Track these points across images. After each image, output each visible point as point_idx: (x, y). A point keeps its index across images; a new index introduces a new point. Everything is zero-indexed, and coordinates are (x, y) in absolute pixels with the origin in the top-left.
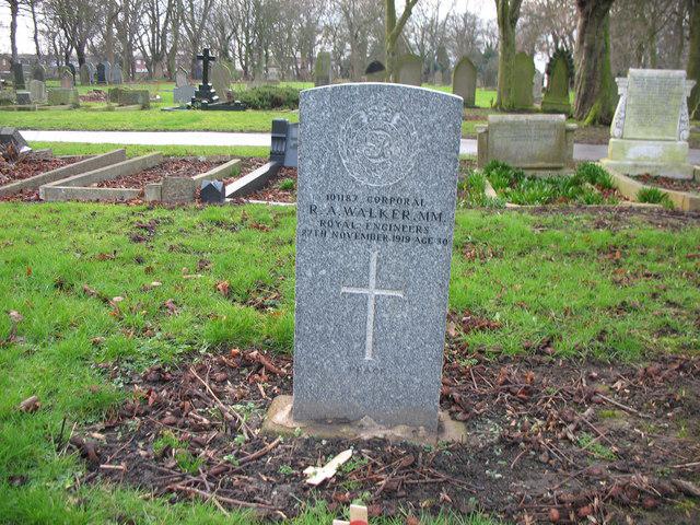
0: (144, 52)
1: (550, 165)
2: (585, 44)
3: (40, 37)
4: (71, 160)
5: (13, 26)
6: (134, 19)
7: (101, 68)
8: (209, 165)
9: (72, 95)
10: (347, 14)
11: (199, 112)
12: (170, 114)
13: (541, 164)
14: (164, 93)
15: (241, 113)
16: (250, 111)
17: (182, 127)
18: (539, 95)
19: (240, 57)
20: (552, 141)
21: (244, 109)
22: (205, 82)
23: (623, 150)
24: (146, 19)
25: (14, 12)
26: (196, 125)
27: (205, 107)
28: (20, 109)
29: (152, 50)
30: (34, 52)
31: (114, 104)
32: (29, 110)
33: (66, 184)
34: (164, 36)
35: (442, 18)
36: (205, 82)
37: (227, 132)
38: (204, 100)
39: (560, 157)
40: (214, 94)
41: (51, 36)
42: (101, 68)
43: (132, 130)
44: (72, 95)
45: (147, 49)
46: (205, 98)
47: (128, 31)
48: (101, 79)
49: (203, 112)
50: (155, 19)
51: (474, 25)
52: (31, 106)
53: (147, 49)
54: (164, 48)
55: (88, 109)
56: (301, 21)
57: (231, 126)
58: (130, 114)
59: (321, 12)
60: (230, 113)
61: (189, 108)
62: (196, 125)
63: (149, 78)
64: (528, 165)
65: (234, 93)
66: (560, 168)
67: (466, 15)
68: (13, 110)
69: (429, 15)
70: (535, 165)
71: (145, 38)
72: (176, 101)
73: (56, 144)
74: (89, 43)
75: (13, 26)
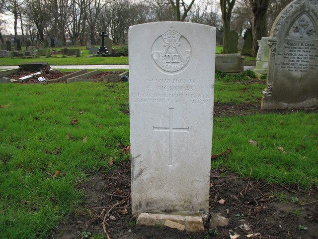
0: (70, 33)
1: (236, 71)
2: (256, 27)
3: (23, 27)
4: (68, 73)
5: (16, 23)
6: (65, 18)
7: (53, 41)
8: (120, 73)
9: (47, 51)
10: (159, 14)
11: (102, 58)
12: (91, 58)
13: (233, 71)
14: (83, 50)
15: (119, 57)
16: (122, 57)
17: (97, 63)
18: (240, 47)
19: (112, 34)
20: (236, 63)
21: (120, 56)
22: (103, 45)
23: (261, 65)
24: (71, 19)
25: (16, 19)
26: (103, 62)
27: (104, 56)
28: (28, 58)
29: (73, 32)
30: (13, 33)
31: (66, 55)
32: (32, 58)
33: (79, 77)
34: (79, 26)
35: (201, 14)
36: (103, 45)
37: (115, 64)
38: (102, 53)
39: (239, 68)
40: (106, 50)
41: (29, 26)
42: (53, 41)
43: (77, 65)
44: (47, 51)
45: (71, 32)
46: (103, 52)
47: (62, 25)
48: (53, 45)
49: (104, 58)
50: (75, 20)
51: (215, 17)
52: (31, 56)
53: (71, 32)
54: (79, 31)
55: (55, 57)
56: (138, 17)
57: (114, 62)
58: (73, 58)
59: (147, 13)
60: (113, 57)
61: (97, 56)
62: (103, 62)
63: (73, 44)
64: (228, 71)
65: (115, 50)
66: (239, 72)
67: (211, 13)
68: (25, 58)
69: (195, 14)
70: (230, 71)
71: (70, 27)
72: (90, 53)
73: (59, 70)
74: (45, 29)
75: (16, 23)
